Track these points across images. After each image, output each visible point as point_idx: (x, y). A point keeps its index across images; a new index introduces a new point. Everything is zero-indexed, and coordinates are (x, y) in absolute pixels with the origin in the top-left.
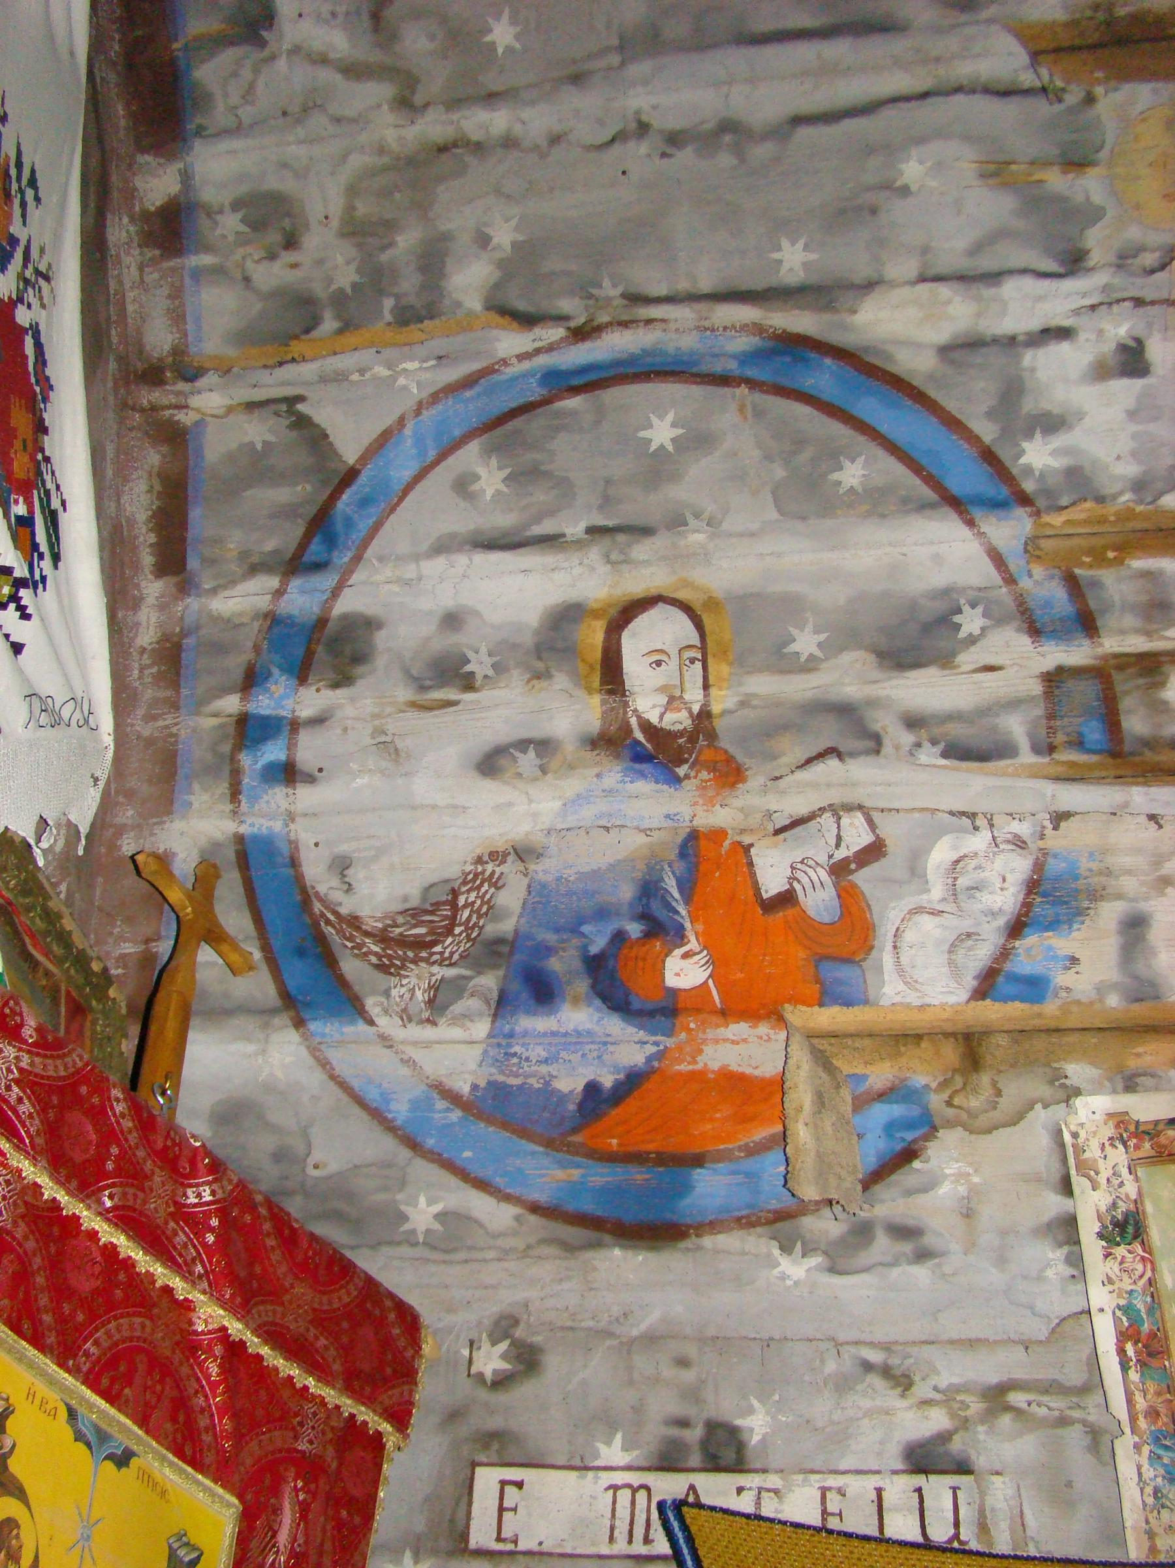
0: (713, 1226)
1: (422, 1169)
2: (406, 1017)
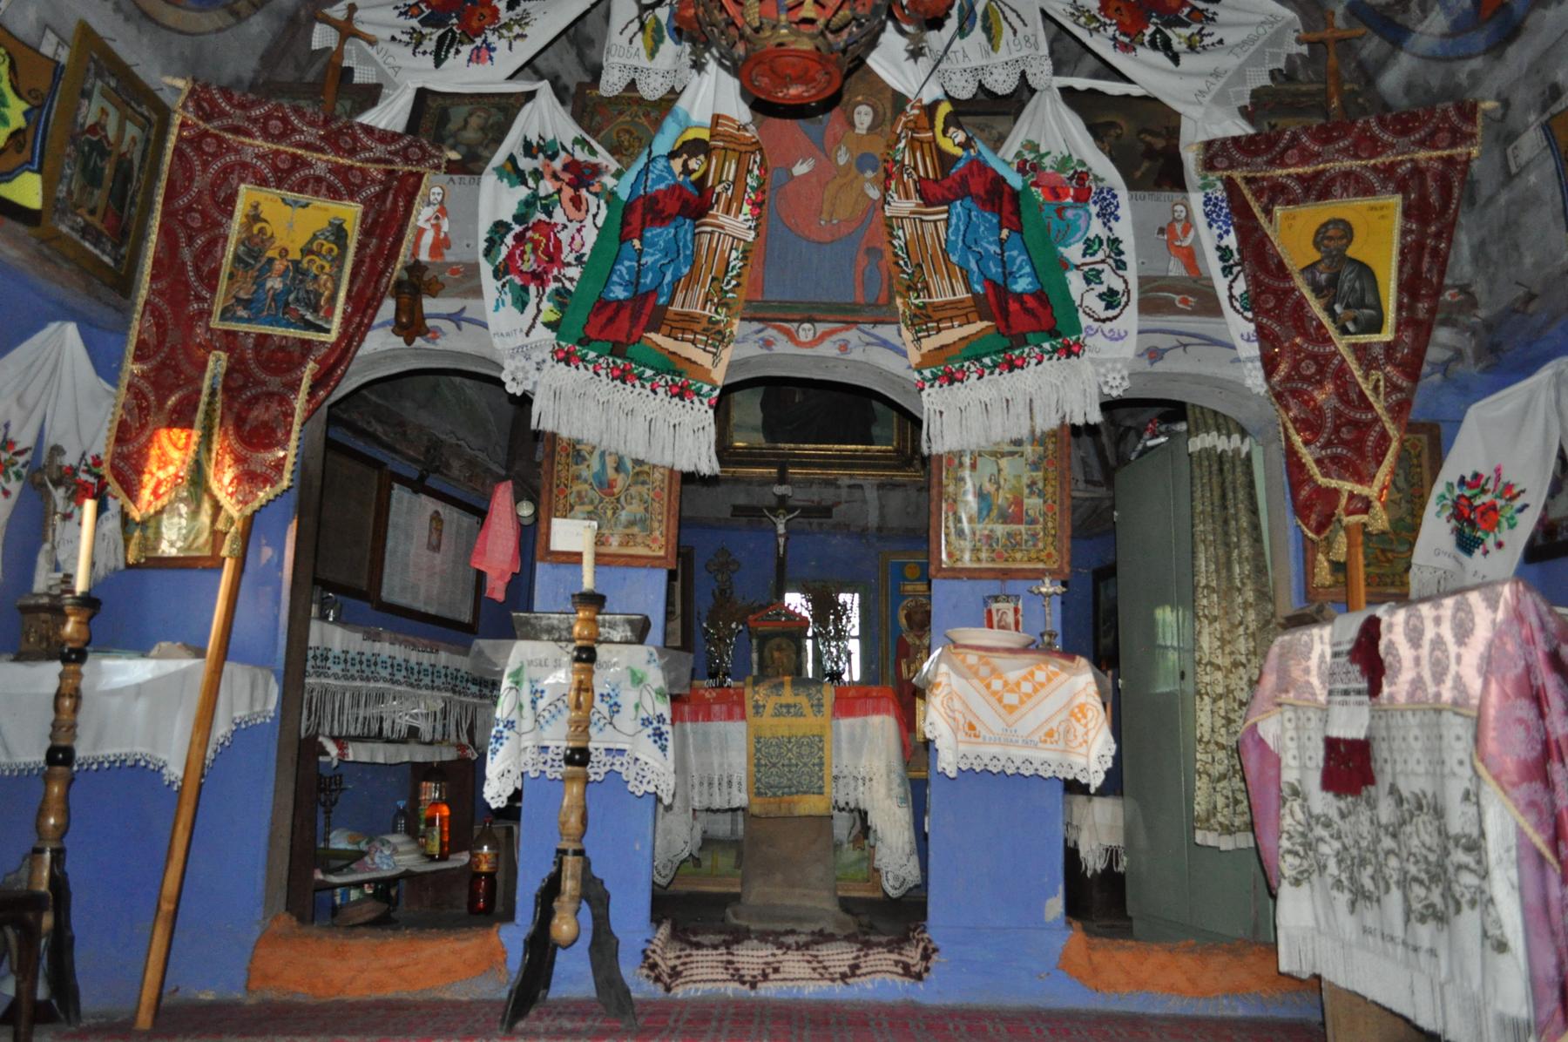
0: (1524, 19)
1: (1456, 65)
2: (1421, 21)
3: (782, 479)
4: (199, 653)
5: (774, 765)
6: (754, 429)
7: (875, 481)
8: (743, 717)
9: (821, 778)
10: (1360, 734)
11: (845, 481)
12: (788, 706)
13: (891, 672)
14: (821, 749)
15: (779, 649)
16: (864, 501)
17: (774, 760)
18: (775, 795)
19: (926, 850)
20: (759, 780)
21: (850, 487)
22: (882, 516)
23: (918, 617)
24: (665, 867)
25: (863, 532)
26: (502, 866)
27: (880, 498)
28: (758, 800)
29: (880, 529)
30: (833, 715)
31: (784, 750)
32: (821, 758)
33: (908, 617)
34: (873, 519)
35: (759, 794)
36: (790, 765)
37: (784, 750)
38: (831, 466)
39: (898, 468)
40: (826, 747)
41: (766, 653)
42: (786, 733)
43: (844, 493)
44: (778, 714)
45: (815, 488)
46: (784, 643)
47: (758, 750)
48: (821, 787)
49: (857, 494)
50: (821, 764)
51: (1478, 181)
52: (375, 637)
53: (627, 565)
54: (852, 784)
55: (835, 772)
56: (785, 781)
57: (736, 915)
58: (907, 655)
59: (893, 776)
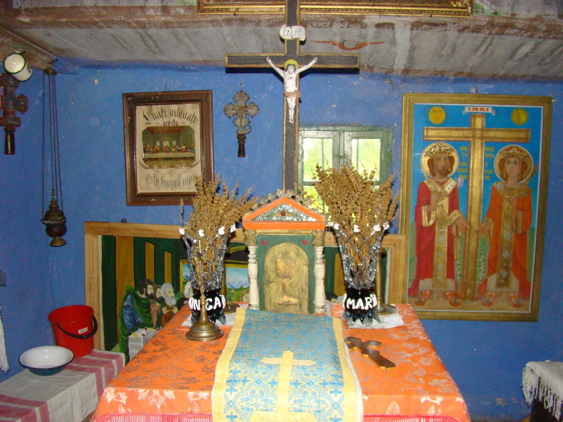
3: (292, 20)
4: (229, 63)
7: (411, 19)
10: (448, 280)
11: (373, 19)
13: (412, 219)
16: (393, 42)
21: (379, 26)
22: (411, 58)
23: (440, 164)
25: (387, 75)
26: (95, 358)
27: (411, 39)
29: (406, 71)
33: (431, 163)
34: (400, 64)
41: (268, 262)
43: (371, 32)
45: (336, 28)
46: (292, 249)
49: (387, 32)
51: (281, 357)
52: (380, 297)
53: (55, 102)
58: (428, 203)
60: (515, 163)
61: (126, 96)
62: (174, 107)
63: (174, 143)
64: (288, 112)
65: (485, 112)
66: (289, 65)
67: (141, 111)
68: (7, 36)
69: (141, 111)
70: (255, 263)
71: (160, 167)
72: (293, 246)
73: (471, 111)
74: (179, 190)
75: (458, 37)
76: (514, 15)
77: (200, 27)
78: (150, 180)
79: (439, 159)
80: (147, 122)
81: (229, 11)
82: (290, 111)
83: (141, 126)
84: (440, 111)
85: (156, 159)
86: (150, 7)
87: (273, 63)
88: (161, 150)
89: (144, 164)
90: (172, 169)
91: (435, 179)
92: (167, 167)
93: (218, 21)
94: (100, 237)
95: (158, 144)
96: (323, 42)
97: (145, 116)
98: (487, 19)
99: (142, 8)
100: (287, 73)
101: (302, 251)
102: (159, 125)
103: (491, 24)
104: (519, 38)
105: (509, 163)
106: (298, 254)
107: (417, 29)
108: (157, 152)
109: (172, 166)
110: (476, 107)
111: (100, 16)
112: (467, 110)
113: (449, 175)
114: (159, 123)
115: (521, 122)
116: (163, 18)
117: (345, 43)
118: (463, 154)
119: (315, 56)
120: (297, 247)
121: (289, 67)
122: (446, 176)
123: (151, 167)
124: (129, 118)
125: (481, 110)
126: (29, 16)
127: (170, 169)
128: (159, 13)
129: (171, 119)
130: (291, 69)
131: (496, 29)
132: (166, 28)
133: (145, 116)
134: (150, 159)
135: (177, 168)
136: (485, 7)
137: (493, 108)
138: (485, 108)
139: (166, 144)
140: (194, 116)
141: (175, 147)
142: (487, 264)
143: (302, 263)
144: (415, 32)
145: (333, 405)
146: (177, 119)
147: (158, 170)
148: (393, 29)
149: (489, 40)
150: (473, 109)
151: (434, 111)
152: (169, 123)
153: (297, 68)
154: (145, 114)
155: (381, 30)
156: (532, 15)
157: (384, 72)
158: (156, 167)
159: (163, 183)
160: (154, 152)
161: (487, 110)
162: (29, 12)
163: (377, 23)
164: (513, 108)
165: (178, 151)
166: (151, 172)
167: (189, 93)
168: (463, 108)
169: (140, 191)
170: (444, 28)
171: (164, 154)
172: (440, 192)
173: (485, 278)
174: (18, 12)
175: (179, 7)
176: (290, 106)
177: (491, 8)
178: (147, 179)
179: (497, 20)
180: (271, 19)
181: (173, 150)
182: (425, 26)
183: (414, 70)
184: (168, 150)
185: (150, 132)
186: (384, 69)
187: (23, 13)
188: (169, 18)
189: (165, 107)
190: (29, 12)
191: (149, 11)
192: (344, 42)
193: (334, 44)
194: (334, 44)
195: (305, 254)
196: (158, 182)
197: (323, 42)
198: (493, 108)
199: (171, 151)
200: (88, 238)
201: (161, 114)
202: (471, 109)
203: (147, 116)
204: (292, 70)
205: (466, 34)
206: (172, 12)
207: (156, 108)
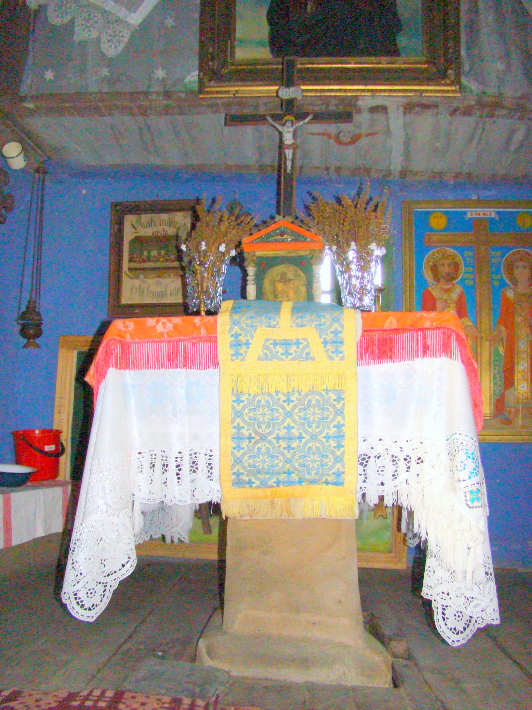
5: (263, 438)
6: (261, 44)
8: (215, 363)
9: (340, 459)
12: (286, 343)
14: (340, 412)
15: (284, 279)
16: (388, 132)
17: (263, 429)
18: (264, 485)
19: (141, 306)
20: (238, 461)
21: (373, 110)
22: (407, 155)
23: (444, 270)
24: (90, 593)
27: (406, 126)
28: (239, 492)
29: (404, 173)
30: (360, 357)
31: (279, 414)
32: (339, 426)
35: (238, 483)
36: (289, 438)
37: (279, 414)
38: (352, 81)
39: (429, 81)
40: (349, 410)
41: (267, 284)
42: (283, 387)
44: (265, 358)
46: (290, 271)
47: (238, 414)
48: (339, 474)
49: (380, 117)
50: (340, 436)
54: (390, 469)
55: (363, 449)
56: (280, 463)
57: (211, 653)
59: (461, 456)
60: (524, 267)
61: (115, 205)
62: (165, 216)
63: (163, 252)
64: (285, 163)
65: (488, 216)
66: (286, 121)
67: (129, 220)
68: (8, 126)
69: (129, 220)
70: (253, 284)
71: (146, 277)
72: (291, 267)
73: (474, 216)
74: (165, 301)
75: (450, 123)
76: (501, 94)
77: (199, 113)
78: (134, 290)
79: (443, 265)
80: (134, 231)
81: (229, 94)
82: (288, 162)
83: (128, 235)
84: (441, 217)
85: (143, 269)
86: (153, 93)
87: (272, 120)
88: (149, 259)
89: (130, 275)
90: (160, 279)
91: (440, 285)
92: (154, 277)
93: (217, 105)
94: (75, 353)
95: (145, 253)
96: (318, 134)
97: (132, 225)
98: (476, 98)
99: (146, 93)
100: (285, 128)
101: (300, 272)
102: (147, 234)
103: (481, 104)
104: (509, 121)
105: (518, 267)
106: (297, 276)
107: (410, 113)
108: (144, 261)
109: (159, 277)
110: (478, 212)
111: (103, 101)
112: (469, 216)
113: (455, 282)
114: (146, 232)
115: (526, 226)
116: (165, 102)
117: (341, 135)
118: (468, 259)
119: (311, 113)
120: (295, 268)
121: (287, 122)
122: (451, 282)
123: (137, 278)
124: (117, 227)
125: (484, 214)
126: (33, 102)
127: (157, 279)
128: (161, 98)
129: (160, 228)
130: (289, 124)
131: (486, 111)
132: (167, 115)
133: (132, 225)
134: (136, 269)
135: (165, 277)
136: (473, 88)
137: (498, 213)
138: (488, 213)
139: (154, 253)
140: (185, 224)
141: (163, 256)
142: (503, 375)
143: (300, 284)
144: (408, 116)
145: (336, 459)
146: (166, 228)
147: (145, 280)
148: (387, 113)
149: (481, 125)
150: (476, 214)
151: (435, 217)
152: (158, 232)
153: (294, 123)
154: (133, 223)
155: (375, 116)
156: (518, 94)
157: (381, 175)
158: (142, 276)
159: (149, 293)
160: (140, 262)
161: (490, 214)
162: (35, 98)
163: (370, 106)
164: (518, 212)
165: (167, 261)
166: (136, 282)
167: (179, 202)
168: (465, 213)
169: (125, 300)
170: (436, 111)
171: (151, 264)
172: (446, 299)
173: (502, 391)
174: (24, 99)
175: (180, 92)
176: (287, 157)
177: (479, 89)
178: (132, 289)
179: (485, 99)
180: (270, 103)
181: (161, 259)
182: (417, 109)
183: (412, 172)
184: (157, 260)
185: (138, 240)
186: (380, 171)
187: (29, 99)
188: (171, 103)
189: (155, 217)
190: (35, 98)
191: (151, 95)
192: (339, 133)
193: (330, 137)
194: (330, 137)
195: (303, 275)
196: (143, 292)
197: (318, 134)
198: (498, 213)
199: (159, 261)
200: (62, 353)
201: (150, 224)
202: (474, 213)
203: (136, 225)
204: (290, 125)
205: (458, 118)
206: (174, 97)
207: (145, 218)
